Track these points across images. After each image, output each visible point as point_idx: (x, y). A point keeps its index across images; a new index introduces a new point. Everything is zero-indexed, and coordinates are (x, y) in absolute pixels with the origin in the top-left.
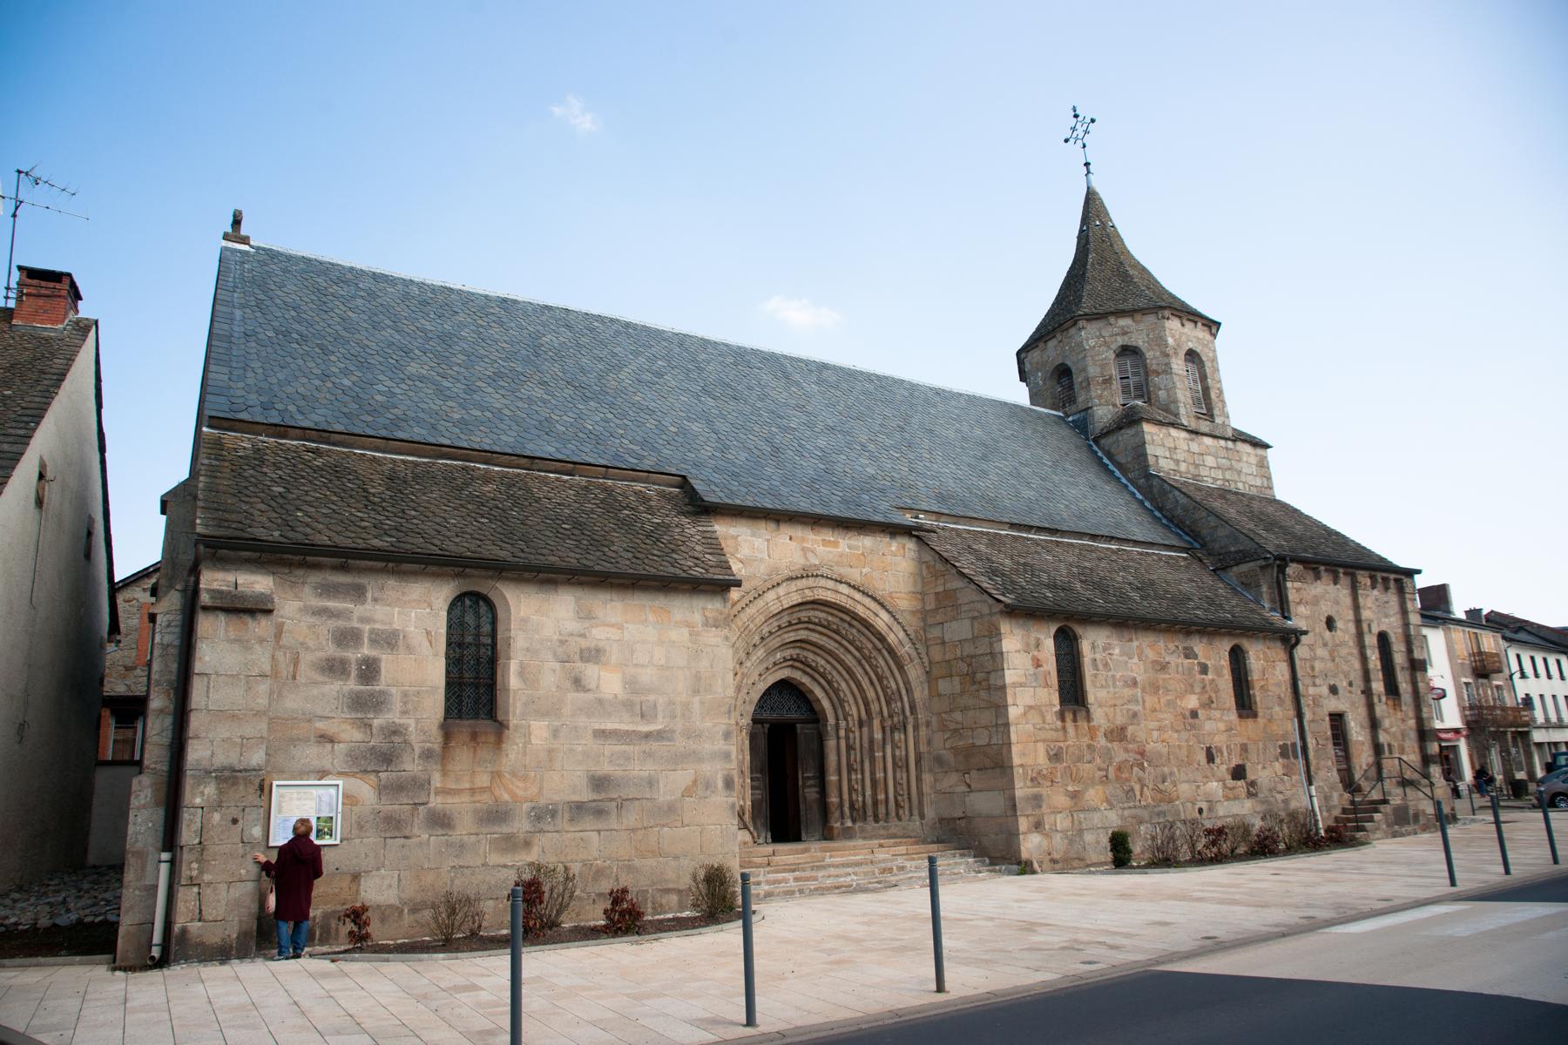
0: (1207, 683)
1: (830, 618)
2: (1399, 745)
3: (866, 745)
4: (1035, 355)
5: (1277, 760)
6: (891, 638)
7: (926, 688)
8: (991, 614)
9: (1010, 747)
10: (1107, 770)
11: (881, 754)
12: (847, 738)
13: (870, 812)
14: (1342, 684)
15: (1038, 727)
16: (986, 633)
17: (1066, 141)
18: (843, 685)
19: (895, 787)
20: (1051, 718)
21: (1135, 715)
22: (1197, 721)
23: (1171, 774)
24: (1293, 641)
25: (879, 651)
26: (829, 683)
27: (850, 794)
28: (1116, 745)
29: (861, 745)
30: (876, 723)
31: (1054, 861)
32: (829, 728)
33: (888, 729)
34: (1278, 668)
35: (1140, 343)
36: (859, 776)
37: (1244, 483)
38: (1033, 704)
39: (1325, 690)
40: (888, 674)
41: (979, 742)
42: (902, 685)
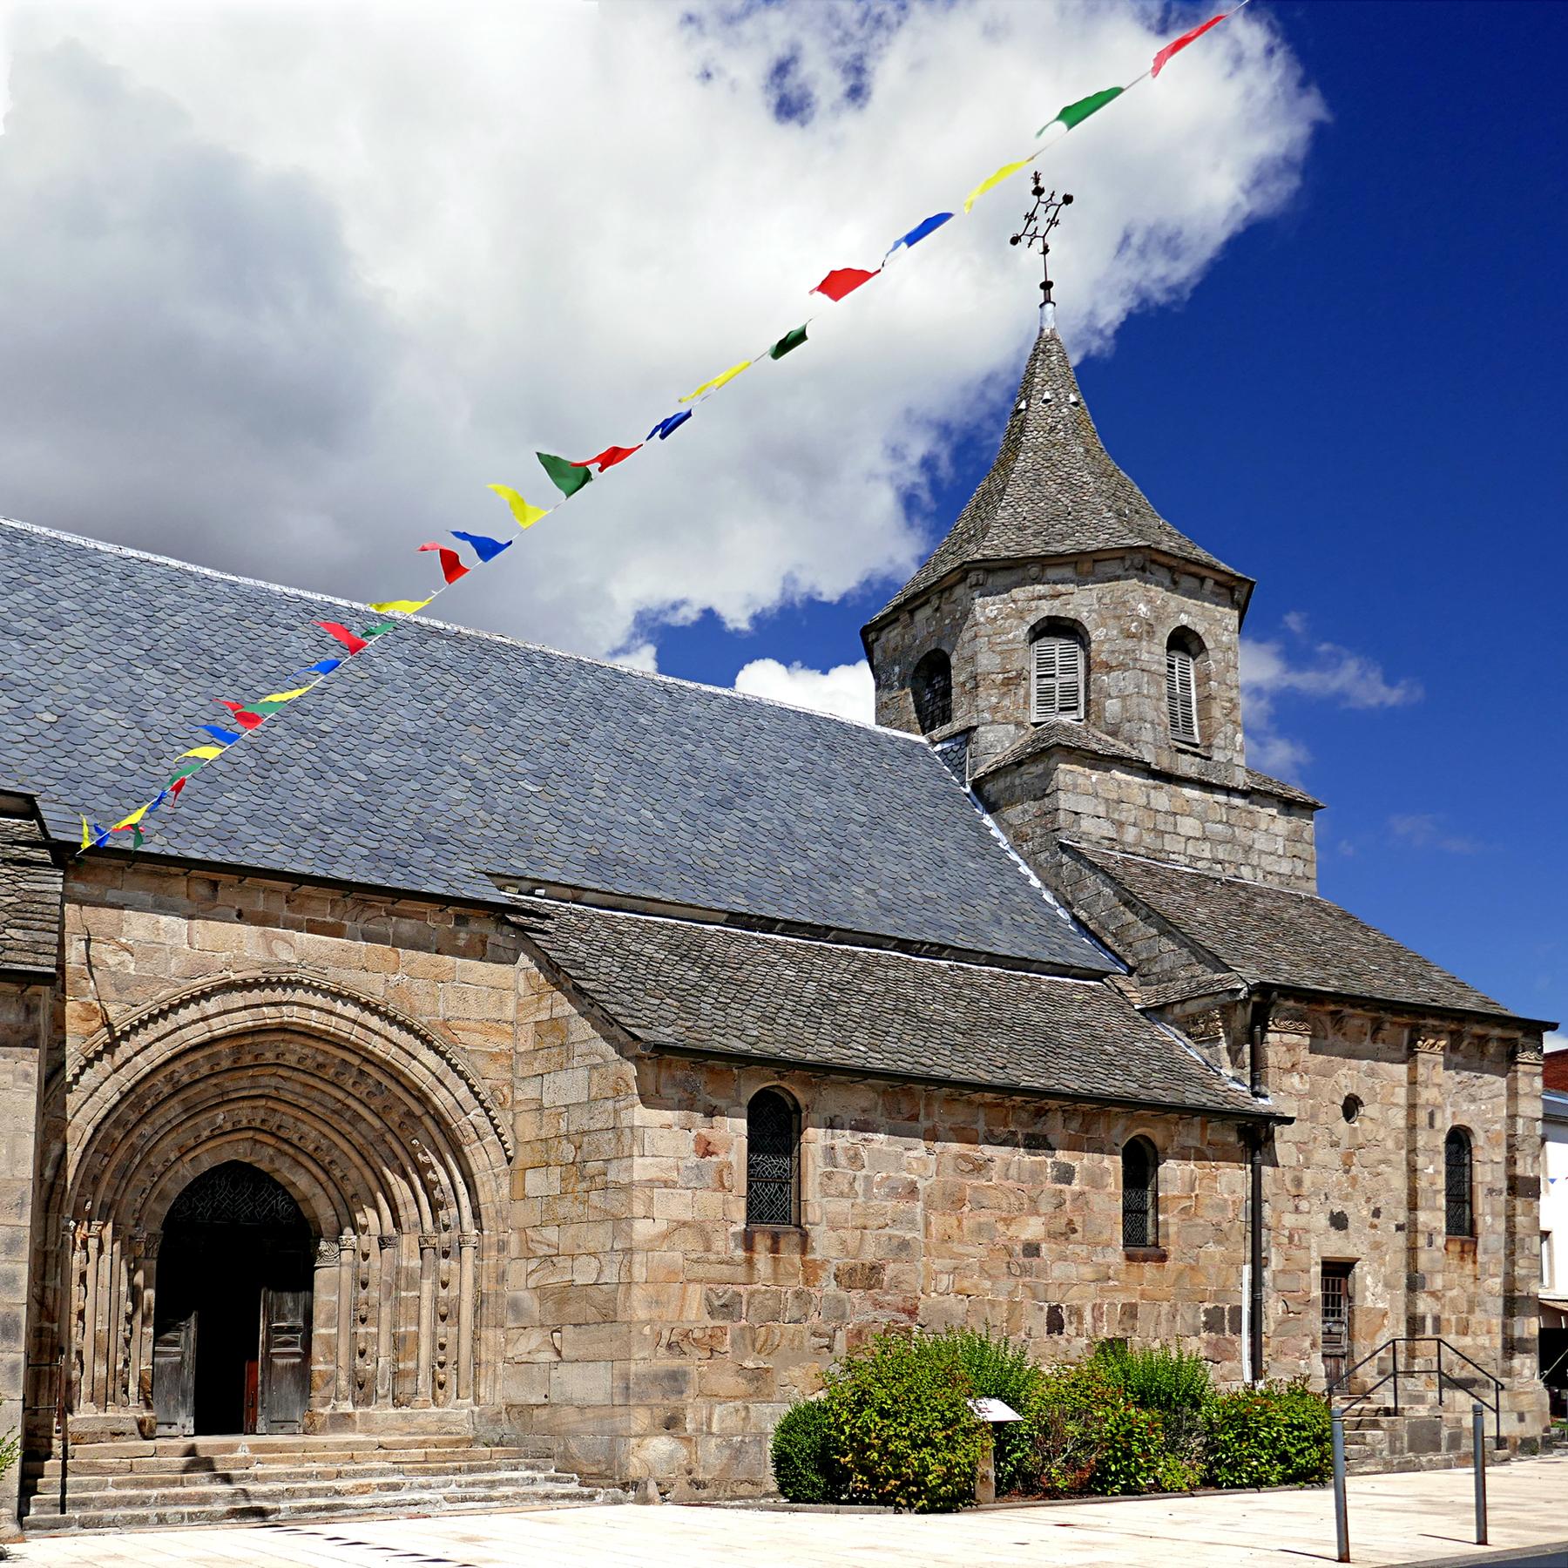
0: (1068, 1197)
2: (1458, 1320)
10: (832, 1338)
14: (1358, 1212)
15: (694, 1256)
16: (610, 1093)
20: (726, 1245)
21: (904, 1245)
22: (1035, 1261)
28: (856, 1295)
31: (700, 1485)
34: (1224, 1180)
35: (1084, 616)
37: (1254, 867)
39: (1322, 1221)
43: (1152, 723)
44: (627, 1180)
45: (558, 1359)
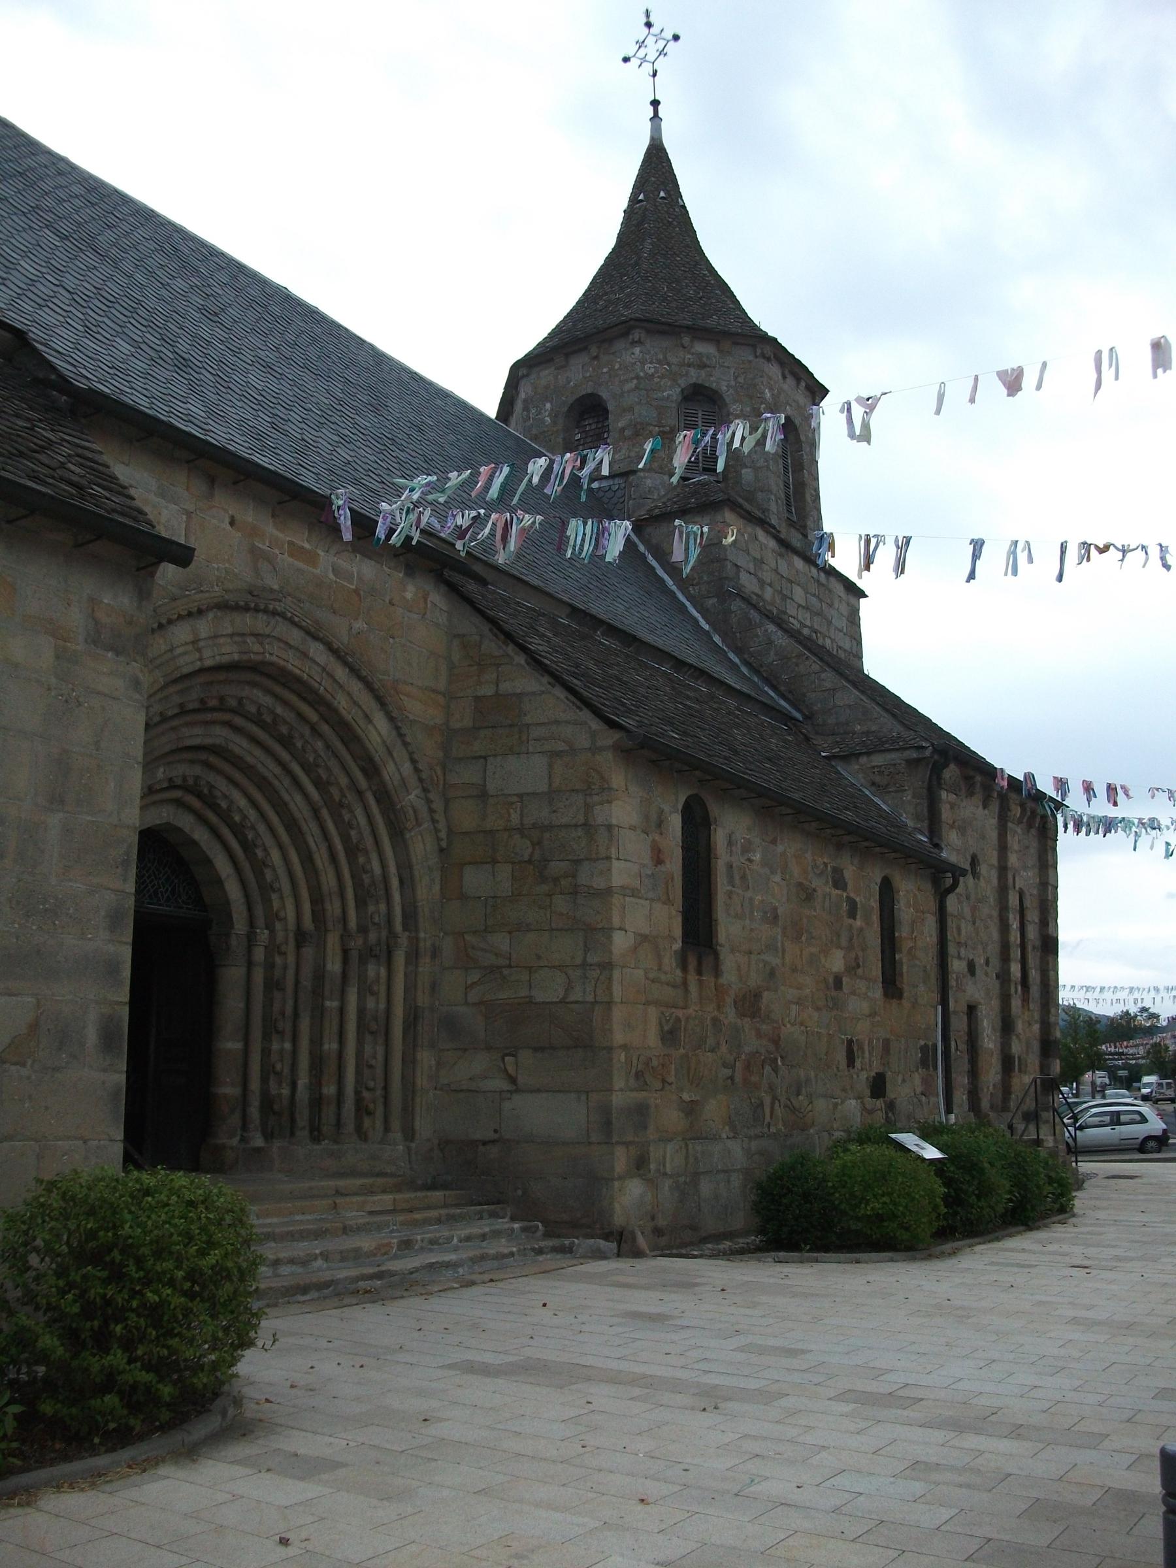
1: (279, 710)
3: (307, 983)
4: (546, 376)
5: (917, 1070)
6: (389, 772)
7: (437, 881)
8: (594, 750)
9: (610, 1009)
10: (733, 1067)
11: (335, 1004)
12: (269, 966)
13: (303, 1120)
15: (651, 976)
17: (626, 60)
18: (275, 856)
19: (359, 1073)
23: (808, 1080)
24: (949, 882)
25: (360, 793)
26: (247, 846)
27: (264, 1080)
29: (297, 983)
30: (333, 941)
32: (234, 942)
33: (354, 954)
36: (288, 1046)
38: (646, 930)
40: (369, 842)
41: (540, 996)
42: (392, 869)
43: (775, 495)
44: (603, 886)
45: (512, 1087)
